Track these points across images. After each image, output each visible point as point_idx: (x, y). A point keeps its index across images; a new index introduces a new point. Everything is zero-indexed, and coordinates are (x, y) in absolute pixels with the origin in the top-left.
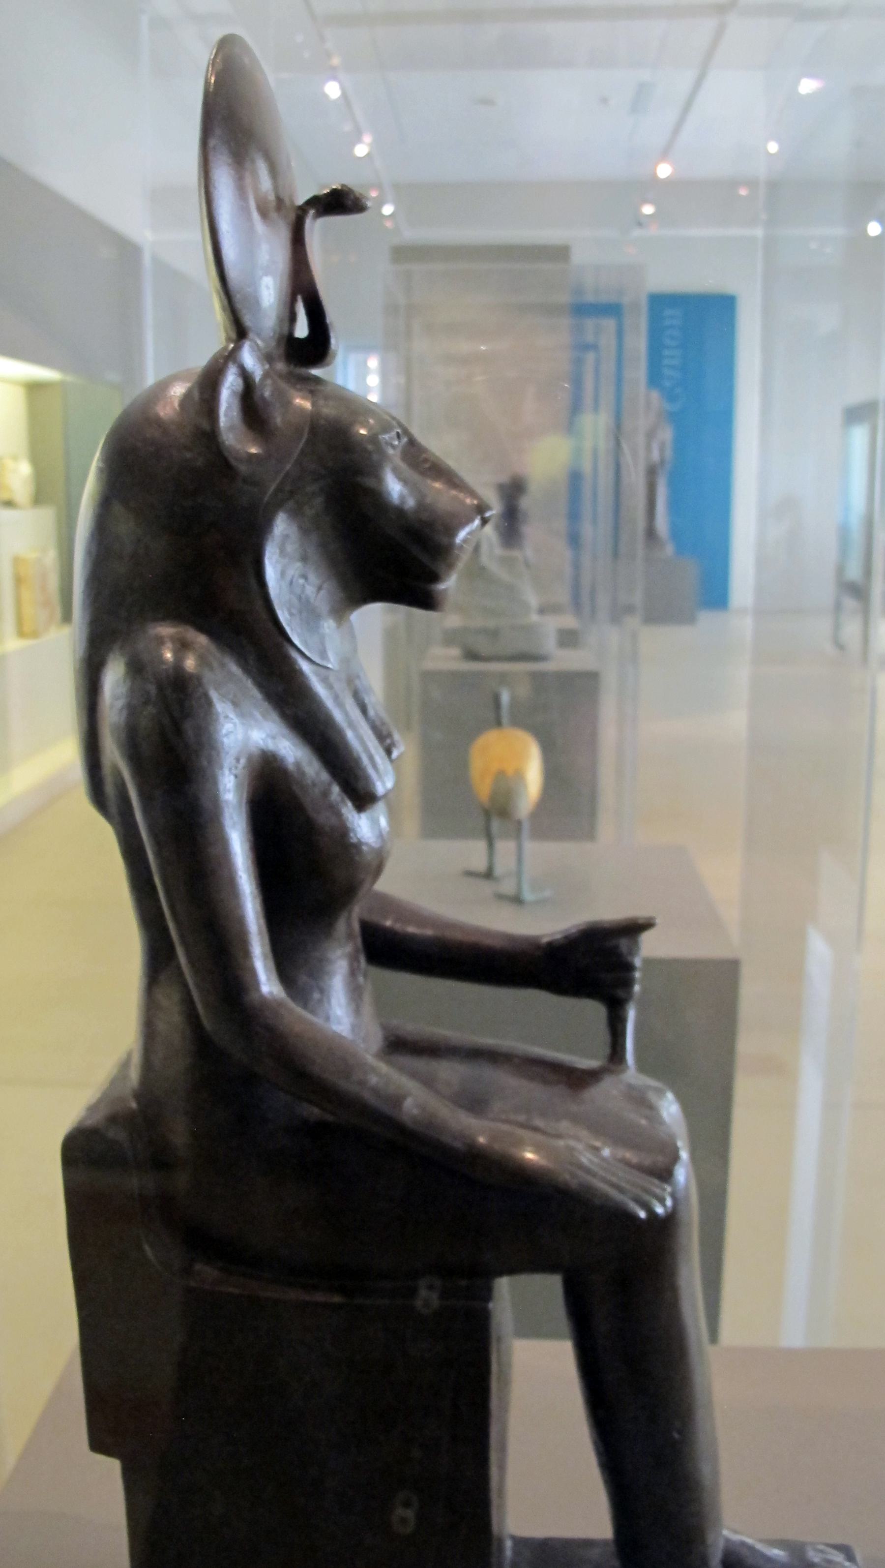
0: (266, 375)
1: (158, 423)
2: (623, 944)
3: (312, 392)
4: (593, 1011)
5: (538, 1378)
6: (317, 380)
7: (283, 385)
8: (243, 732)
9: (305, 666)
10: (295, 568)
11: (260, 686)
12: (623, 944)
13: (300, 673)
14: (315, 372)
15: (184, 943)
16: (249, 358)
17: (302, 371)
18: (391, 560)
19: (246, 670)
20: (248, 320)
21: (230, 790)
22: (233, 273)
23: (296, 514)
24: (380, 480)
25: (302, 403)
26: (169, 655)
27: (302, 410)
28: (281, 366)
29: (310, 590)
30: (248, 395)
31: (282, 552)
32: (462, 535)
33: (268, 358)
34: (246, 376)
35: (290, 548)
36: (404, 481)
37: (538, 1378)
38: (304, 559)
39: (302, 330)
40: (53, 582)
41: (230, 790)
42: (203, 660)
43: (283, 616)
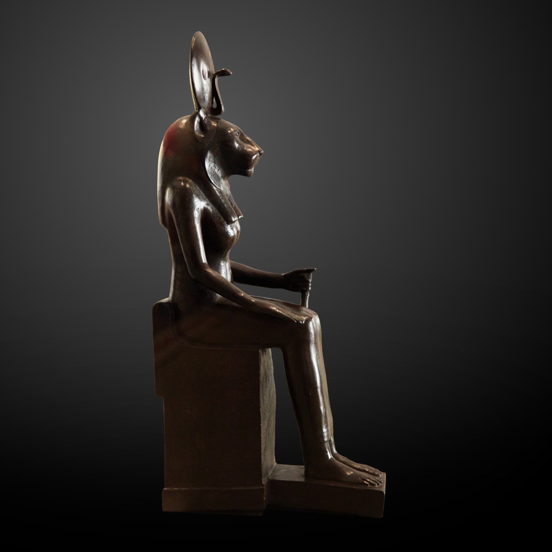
0: (206, 118)
1: (180, 129)
2: (306, 275)
3: (217, 122)
4: (299, 294)
5: (268, 360)
6: (219, 119)
7: (210, 120)
8: (200, 204)
9: (214, 188)
10: (212, 165)
11: (204, 193)
12: (306, 275)
13: (214, 189)
14: (218, 116)
15: (182, 243)
16: (202, 113)
17: (215, 116)
18: (236, 164)
19: (201, 188)
20: (201, 105)
21: (197, 215)
22: (198, 94)
23: (212, 152)
24: (233, 143)
25: (214, 124)
26: (182, 184)
27: (214, 126)
28: (209, 115)
29: (216, 170)
30: (201, 122)
31: (209, 160)
32: (254, 157)
33: (206, 114)
34: (201, 118)
35: (211, 160)
36: (239, 144)
37: (268, 360)
38: (215, 162)
39: (215, 106)
40: (265, 397)
41: (197, 215)
42: (190, 184)
43: (209, 176)
